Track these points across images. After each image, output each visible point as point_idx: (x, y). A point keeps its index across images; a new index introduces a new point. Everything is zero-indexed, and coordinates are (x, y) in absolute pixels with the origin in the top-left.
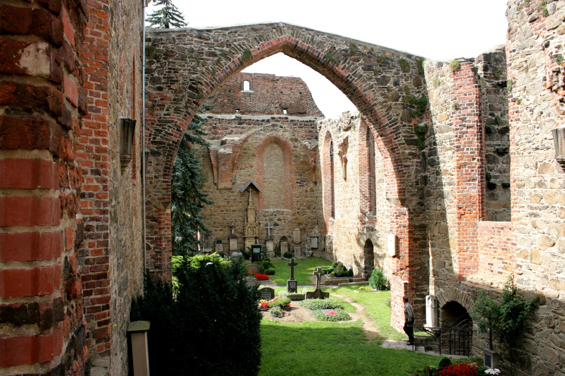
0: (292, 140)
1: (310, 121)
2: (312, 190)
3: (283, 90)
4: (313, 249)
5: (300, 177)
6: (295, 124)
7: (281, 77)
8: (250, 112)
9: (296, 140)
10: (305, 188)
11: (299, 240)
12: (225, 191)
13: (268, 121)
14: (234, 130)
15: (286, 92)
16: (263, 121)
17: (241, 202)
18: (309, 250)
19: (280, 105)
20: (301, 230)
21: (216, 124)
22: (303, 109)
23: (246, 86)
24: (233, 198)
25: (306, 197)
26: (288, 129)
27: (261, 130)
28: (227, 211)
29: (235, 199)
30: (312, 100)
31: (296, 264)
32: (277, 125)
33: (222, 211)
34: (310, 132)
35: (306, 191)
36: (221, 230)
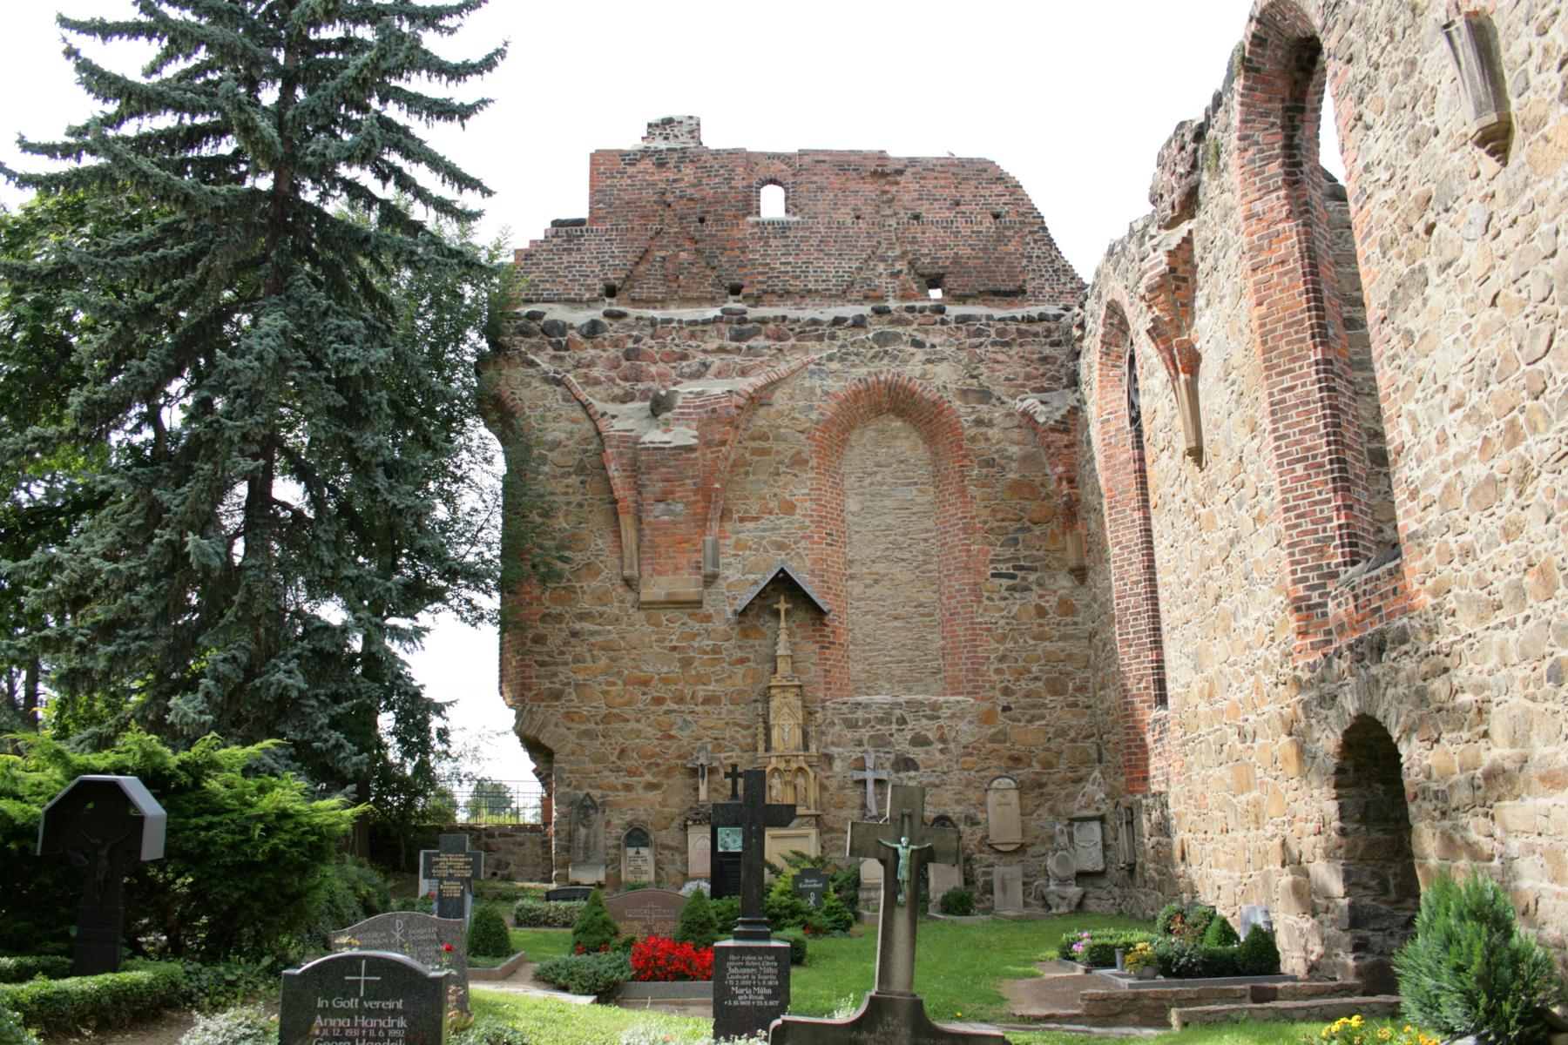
0: (964, 393)
1: (1042, 318)
2: (1066, 607)
3: (923, 208)
4: (1082, 876)
5: (1009, 552)
6: (979, 333)
7: (913, 161)
8: (785, 295)
9: (985, 395)
10: (1033, 598)
11: (1016, 837)
12: (670, 614)
13: (859, 322)
14: (716, 361)
15: (935, 212)
16: (838, 321)
17: (742, 661)
18: (1063, 882)
19: (911, 264)
20: (1022, 788)
21: (637, 340)
22: (1012, 277)
24: (707, 643)
25: (1040, 637)
26: (949, 351)
27: (830, 358)
28: (681, 700)
29: (716, 650)
30: (1050, 242)
31: (734, 766)
32: (897, 337)
33: (659, 701)
34: (1045, 360)
35: (1041, 612)
36: (651, 787)
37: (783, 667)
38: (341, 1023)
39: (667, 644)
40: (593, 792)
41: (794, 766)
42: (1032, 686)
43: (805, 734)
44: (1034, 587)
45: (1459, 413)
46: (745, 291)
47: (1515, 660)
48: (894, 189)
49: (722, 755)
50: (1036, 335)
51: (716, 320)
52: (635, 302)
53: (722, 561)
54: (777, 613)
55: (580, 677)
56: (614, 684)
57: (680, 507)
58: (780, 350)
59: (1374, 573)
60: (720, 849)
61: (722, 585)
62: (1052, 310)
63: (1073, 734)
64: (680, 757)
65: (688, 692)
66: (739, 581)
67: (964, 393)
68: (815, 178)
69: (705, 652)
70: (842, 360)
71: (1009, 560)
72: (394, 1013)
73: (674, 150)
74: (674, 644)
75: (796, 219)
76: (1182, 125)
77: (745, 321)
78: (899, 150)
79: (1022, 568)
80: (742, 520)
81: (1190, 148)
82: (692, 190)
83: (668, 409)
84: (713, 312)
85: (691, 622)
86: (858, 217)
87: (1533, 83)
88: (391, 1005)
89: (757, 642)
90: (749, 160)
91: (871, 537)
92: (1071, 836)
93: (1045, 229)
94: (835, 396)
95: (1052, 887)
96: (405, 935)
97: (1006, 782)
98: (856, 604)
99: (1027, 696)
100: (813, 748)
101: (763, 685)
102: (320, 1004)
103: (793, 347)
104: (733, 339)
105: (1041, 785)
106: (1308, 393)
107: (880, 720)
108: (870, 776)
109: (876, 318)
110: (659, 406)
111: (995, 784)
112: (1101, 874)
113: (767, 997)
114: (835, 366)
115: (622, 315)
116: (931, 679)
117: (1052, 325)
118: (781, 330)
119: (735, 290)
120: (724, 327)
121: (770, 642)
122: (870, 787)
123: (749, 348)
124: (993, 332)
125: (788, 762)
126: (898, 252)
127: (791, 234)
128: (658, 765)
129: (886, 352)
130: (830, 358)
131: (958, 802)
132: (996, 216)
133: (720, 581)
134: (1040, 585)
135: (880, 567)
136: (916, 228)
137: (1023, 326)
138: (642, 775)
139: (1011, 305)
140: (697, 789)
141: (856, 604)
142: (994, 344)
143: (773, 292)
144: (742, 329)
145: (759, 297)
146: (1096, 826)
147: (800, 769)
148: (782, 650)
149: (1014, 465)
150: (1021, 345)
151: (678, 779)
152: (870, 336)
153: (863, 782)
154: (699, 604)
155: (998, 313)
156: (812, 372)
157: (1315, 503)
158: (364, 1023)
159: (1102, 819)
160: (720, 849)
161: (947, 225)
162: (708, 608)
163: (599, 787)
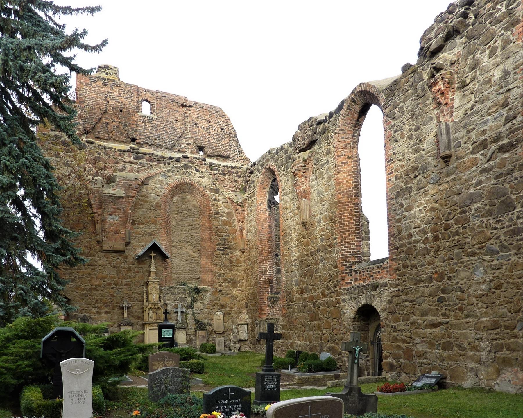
0: (211, 190)
1: (236, 167)
3: (198, 122)
4: (241, 341)
6: (216, 170)
7: (196, 103)
8: (152, 145)
9: (217, 191)
11: (222, 329)
12: (113, 254)
13: (178, 160)
15: (203, 124)
16: (171, 158)
17: (138, 272)
18: (235, 343)
23: (146, 109)
27: (169, 171)
29: (129, 268)
32: (191, 167)
33: (109, 284)
34: (236, 181)
36: (106, 313)
37: (153, 275)
38: (224, 407)
39: (112, 265)
40: (86, 315)
41: (157, 307)
42: (228, 284)
43: (160, 296)
44: (229, 254)
45: (417, 230)
46: (137, 141)
47: (427, 295)
48: (189, 112)
49: (132, 303)
50: (233, 173)
51: (128, 151)
52: (97, 138)
53: (132, 238)
54: (151, 257)
55: (81, 275)
56: (93, 278)
57: (116, 218)
58: (151, 166)
59: (372, 266)
60: (163, 336)
61: (131, 246)
62: (238, 165)
63: (238, 299)
64: (117, 303)
65: (120, 281)
66: (137, 245)
67: (211, 190)
68: (162, 103)
69: (126, 269)
70: (172, 172)
71: (222, 245)
72: (238, 403)
73: (110, 80)
74: (115, 265)
75: (156, 117)
76: (311, 118)
77: (139, 153)
78: (192, 98)
79: (226, 248)
80: (138, 224)
81: (315, 126)
82: (118, 98)
83: (114, 182)
84: (126, 147)
85: (120, 258)
86: (177, 121)
87: (462, 145)
88: (237, 401)
89: (143, 266)
90: (138, 91)
91: (180, 234)
92: (237, 329)
93: (236, 137)
94: (170, 185)
95: (232, 344)
96: (172, 374)
97: (219, 313)
98: (174, 255)
99: (226, 287)
100: (162, 301)
101: (145, 280)
102: (217, 403)
103: (156, 165)
104: (134, 159)
105: (229, 314)
106: (352, 212)
107: (183, 293)
108: (179, 310)
109: (183, 159)
110: (110, 180)
111: (217, 313)
112: (247, 340)
113: (275, 388)
114: (170, 174)
115: (93, 143)
116: (197, 281)
117: (239, 170)
118: (152, 158)
119: (133, 140)
120: (132, 155)
121: (147, 266)
122: (179, 314)
123: (140, 163)
124: (220, 169)
125: (155, 306)
126: (190, 136)
127: (154, 122)
128: (109, 306)
129: (187, 172)
130: (169, 171)
131: (205, 319)
132: (222, 129)
133: (130, 245)
134: (231, 253)
135: (182, 244)
136: (196, 129)
137: (230, 169)
138: (104, 309)
139: (225, 161)
140: (123, 314)
141: (174, 255)
142: (220, 174)
143: (147, 144)
144: (138, 155)
145: (142, 144)
146: (246, 326)
147: (158, 308)
148: (153, 269)
149: (225, 215)
150: (229, 176)
151: (116, 310)
152: (182, 165)
153: (177, 312)
154: (123, 252)
155: (223, 164)
156: (162, 175)
157: (351, 244)
158: (230, 407)
159: (247, 324)
160: (163, 336)
161: (207, 129)
162: (126, 253)
163: (88, 313)
